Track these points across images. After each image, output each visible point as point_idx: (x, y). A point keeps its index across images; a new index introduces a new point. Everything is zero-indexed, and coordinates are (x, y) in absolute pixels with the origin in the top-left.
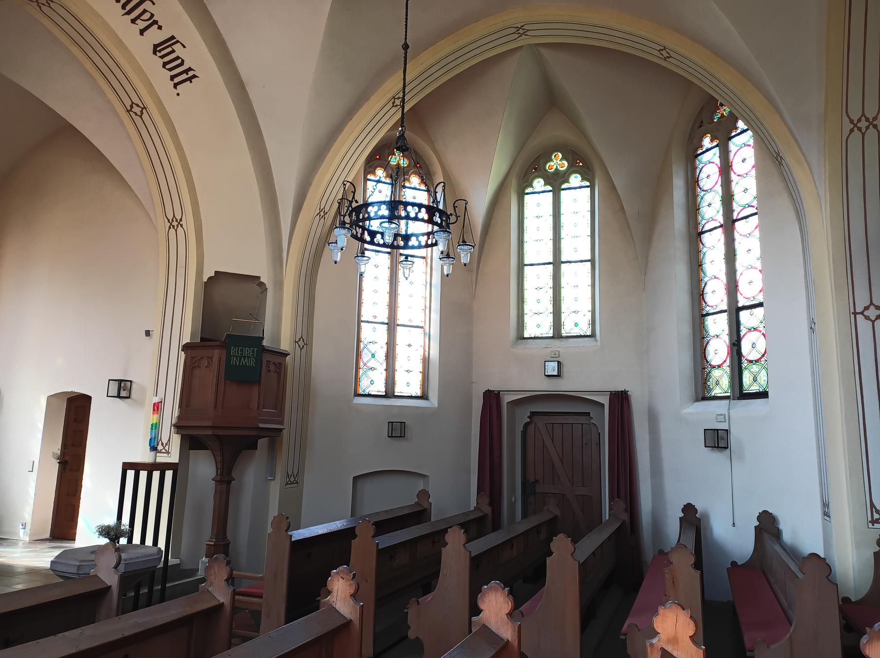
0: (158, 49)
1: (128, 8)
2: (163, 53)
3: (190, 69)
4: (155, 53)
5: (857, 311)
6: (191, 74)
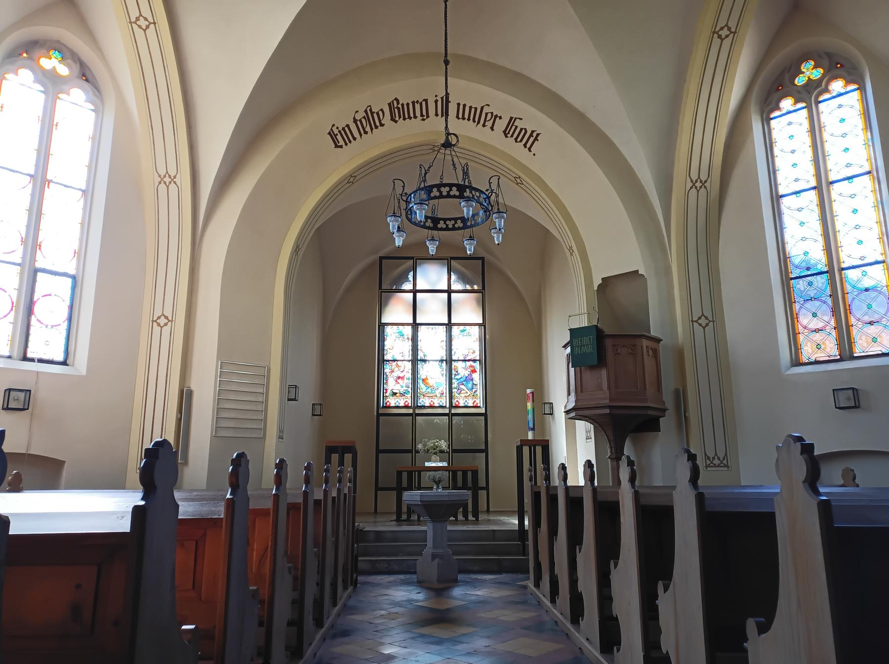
0: (507, 133)
1: (477, 120)
2: (511, 133)
3: (533, 132)
4: (506, 137)
5: (38, 273)
6: (535, 135)
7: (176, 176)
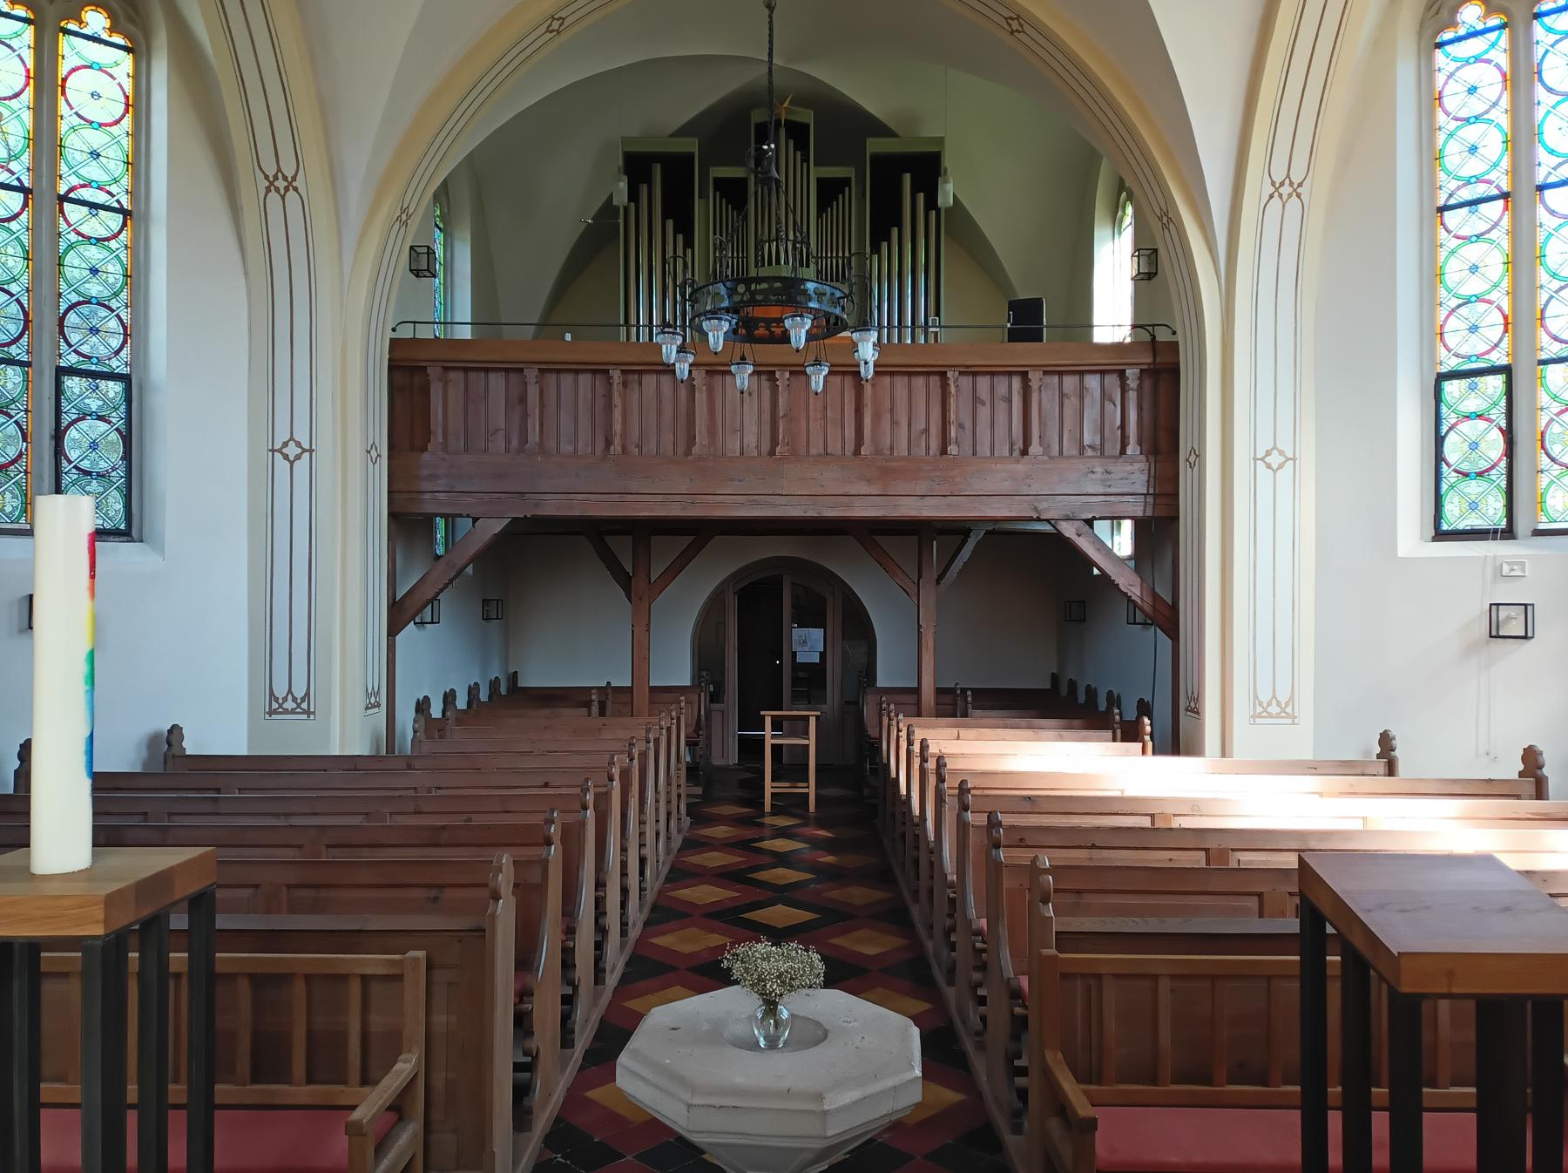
7: (1302, 183)
